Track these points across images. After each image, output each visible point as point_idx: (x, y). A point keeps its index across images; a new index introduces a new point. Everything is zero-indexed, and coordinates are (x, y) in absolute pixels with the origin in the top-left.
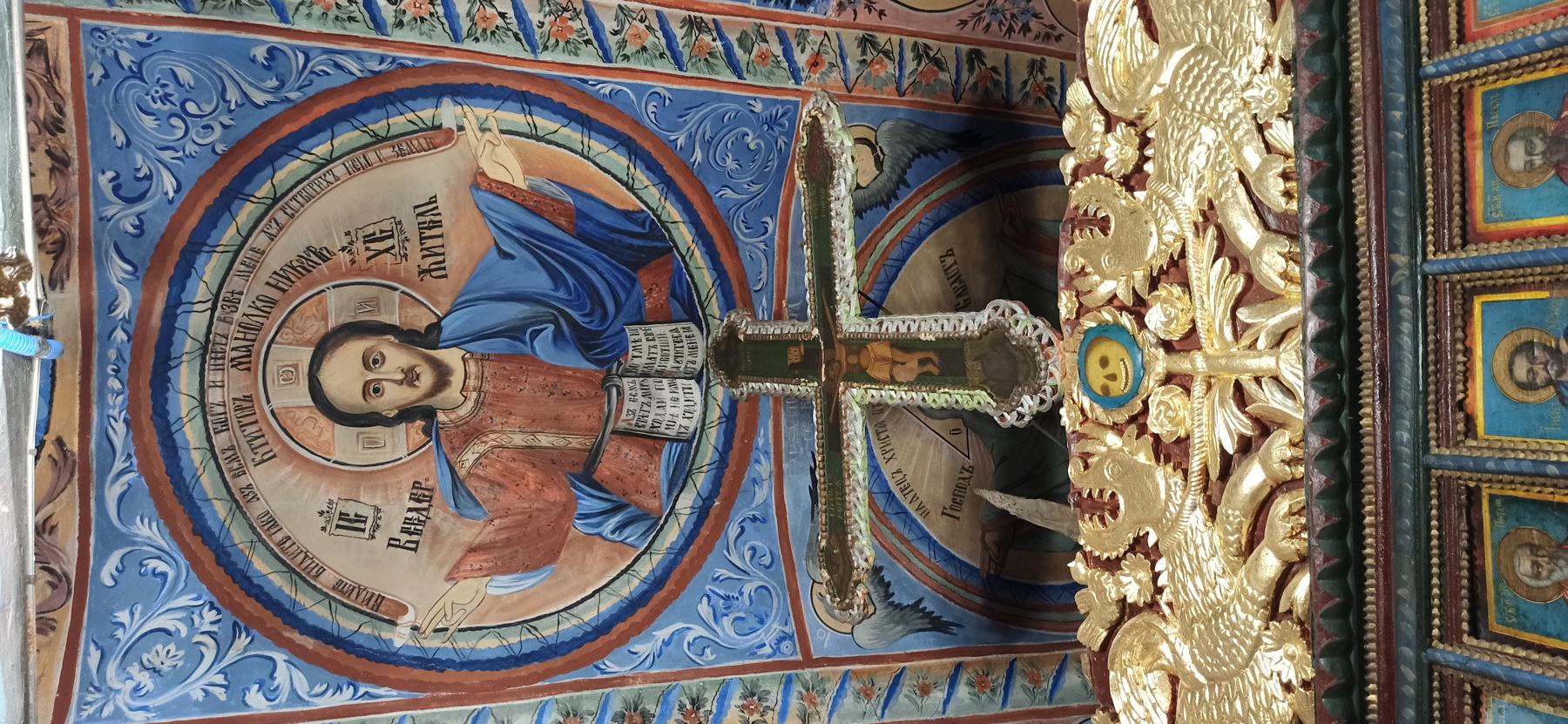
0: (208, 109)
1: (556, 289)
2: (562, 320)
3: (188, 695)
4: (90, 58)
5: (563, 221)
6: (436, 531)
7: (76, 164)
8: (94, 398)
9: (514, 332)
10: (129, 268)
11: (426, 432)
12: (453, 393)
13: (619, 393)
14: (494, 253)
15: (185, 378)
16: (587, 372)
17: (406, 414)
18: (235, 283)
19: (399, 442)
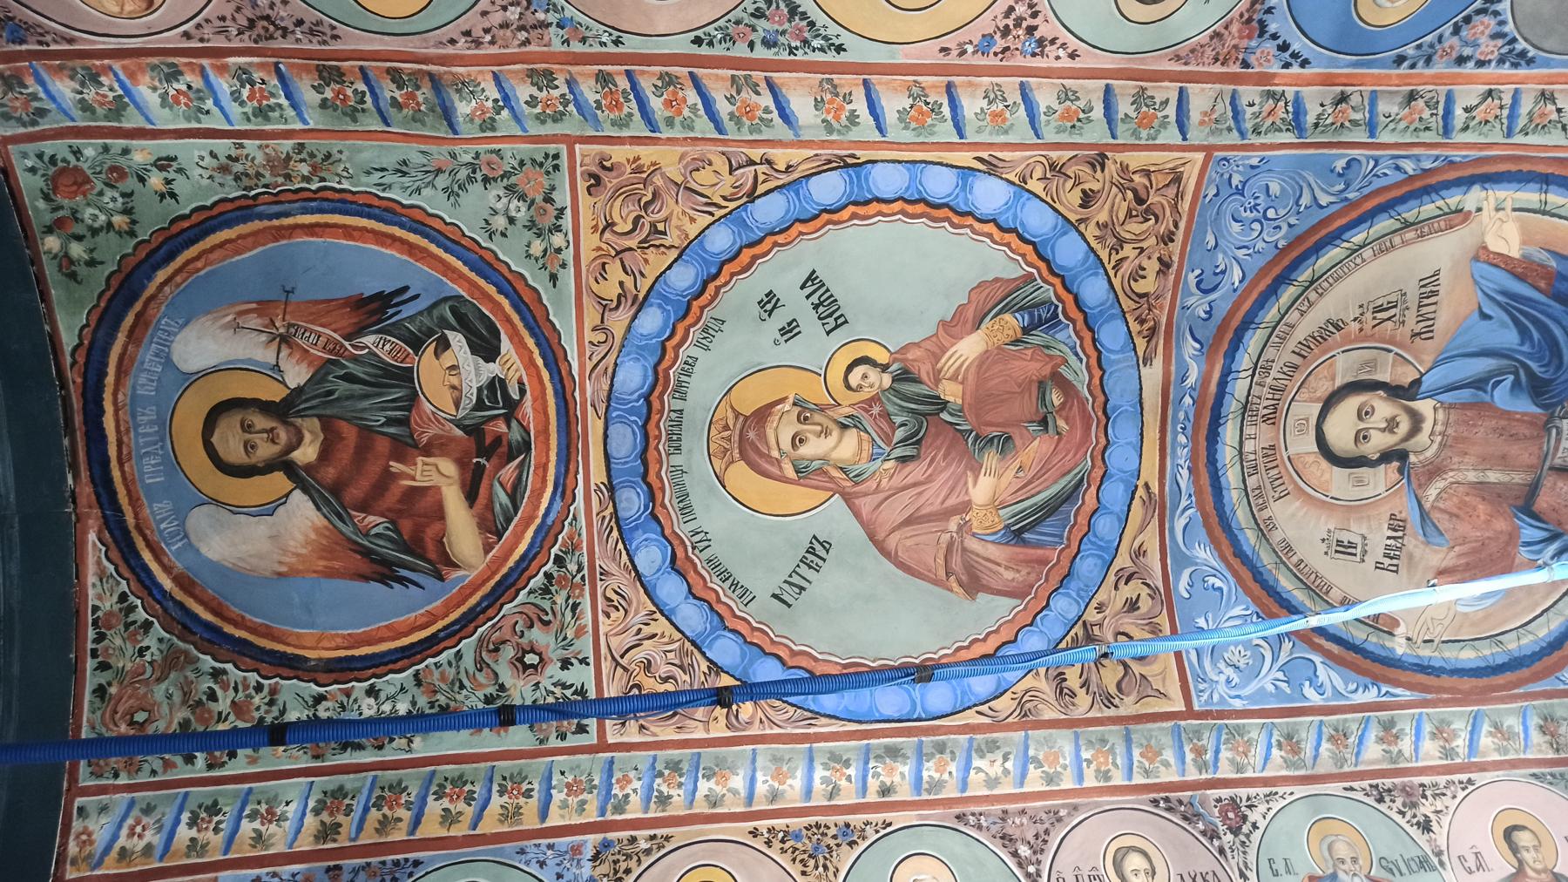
0: (1282, 212)
1: (1522, 344)
2: (1522, 372)
3: (1263, 688)
4: (1211, 181)
5: (1542, 284)
6: (1411, 557)
7: (1175, 266)
8: (1169, 451)
9: (1479, 384)
10: (1197, 346)
11: (1401, 471)
12: (1423, 438)
13: (1558, 433)
14: (1476, 315)
15: (1229, 433)
16: (1533, 415)
17: (1386, 457)
18: (1270, 353)
19: (1380, 479)
